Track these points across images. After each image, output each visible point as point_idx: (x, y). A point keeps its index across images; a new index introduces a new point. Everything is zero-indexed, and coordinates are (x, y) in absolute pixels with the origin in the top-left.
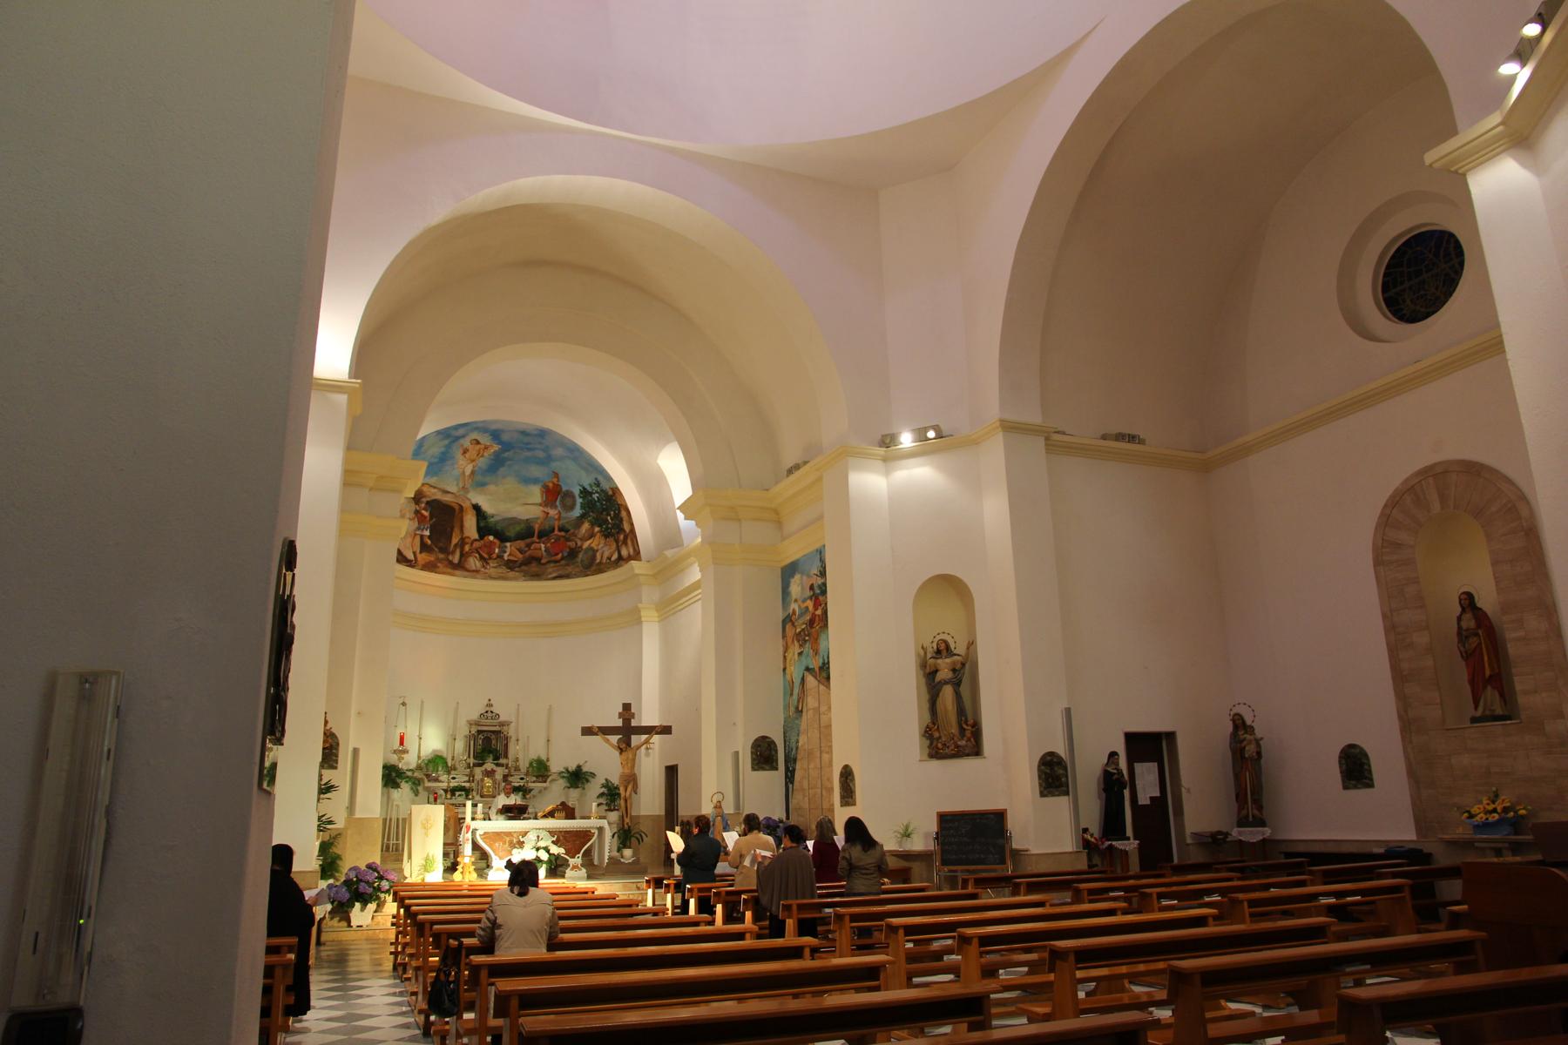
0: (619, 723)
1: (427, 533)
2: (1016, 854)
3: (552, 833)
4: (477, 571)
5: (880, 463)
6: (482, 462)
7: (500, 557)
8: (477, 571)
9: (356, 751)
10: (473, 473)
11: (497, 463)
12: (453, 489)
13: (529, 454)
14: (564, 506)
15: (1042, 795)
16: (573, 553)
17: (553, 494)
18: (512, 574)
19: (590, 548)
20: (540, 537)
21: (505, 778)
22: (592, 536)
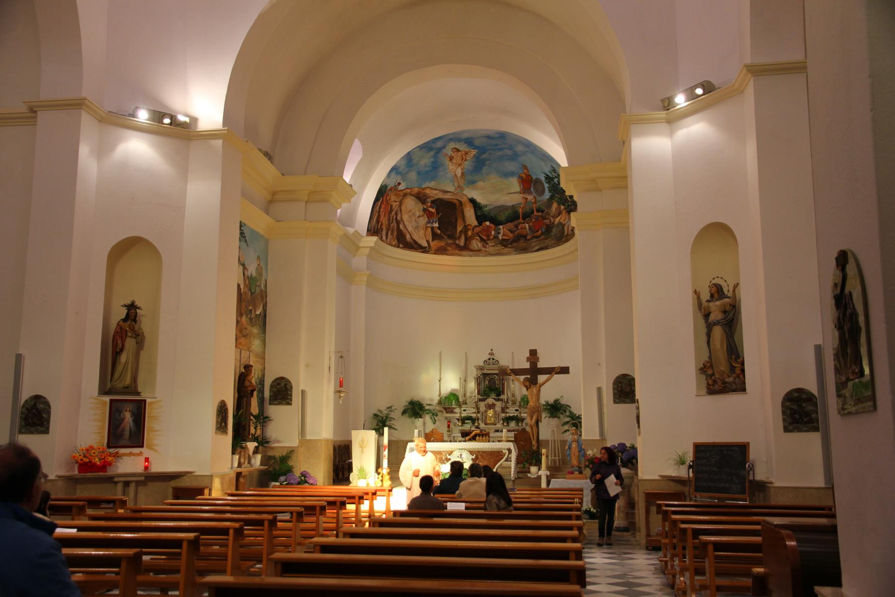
0: (527, 365)
1: (436, 225)
2: (762, 487)
3: (471, 452)
4: (479, 251)
5: (665, 126)
6: (468, 165)
7: (496, 237)
8: (479, 251)
9: (303, 392)
10: (463, 174)
11: (479, 165)
12: (451, 189)
13: (500, 153)
14: (537, 191)
15: (786, 430)
16: (549, 228)
17: (528, 183)
18: (506, 250)
19: (560, 223)
20: (524, 219)
21: (503, 410)
22: (560, 213)
